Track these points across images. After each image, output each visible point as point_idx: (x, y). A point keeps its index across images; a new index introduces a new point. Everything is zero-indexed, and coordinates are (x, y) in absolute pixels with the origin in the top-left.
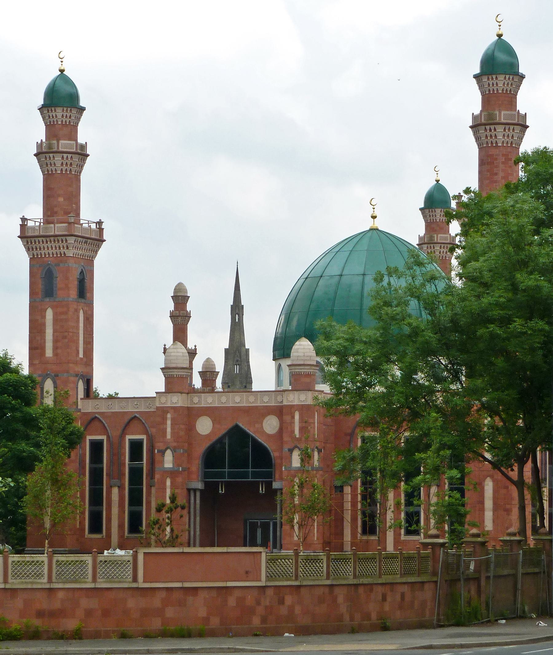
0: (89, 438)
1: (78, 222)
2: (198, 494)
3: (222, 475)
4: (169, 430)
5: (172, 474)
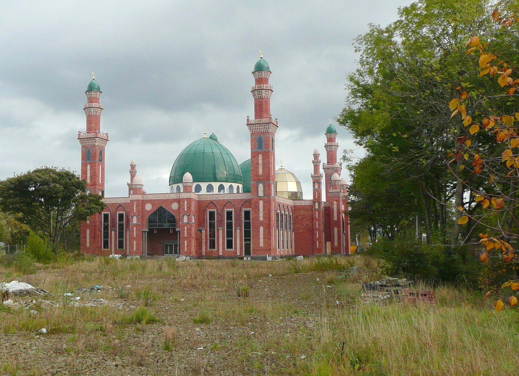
0: (103, 213)
1: (99, 133)
2: (146, 233)
3: (156, 226)
4: (135, 209)
5: (137, 225)
